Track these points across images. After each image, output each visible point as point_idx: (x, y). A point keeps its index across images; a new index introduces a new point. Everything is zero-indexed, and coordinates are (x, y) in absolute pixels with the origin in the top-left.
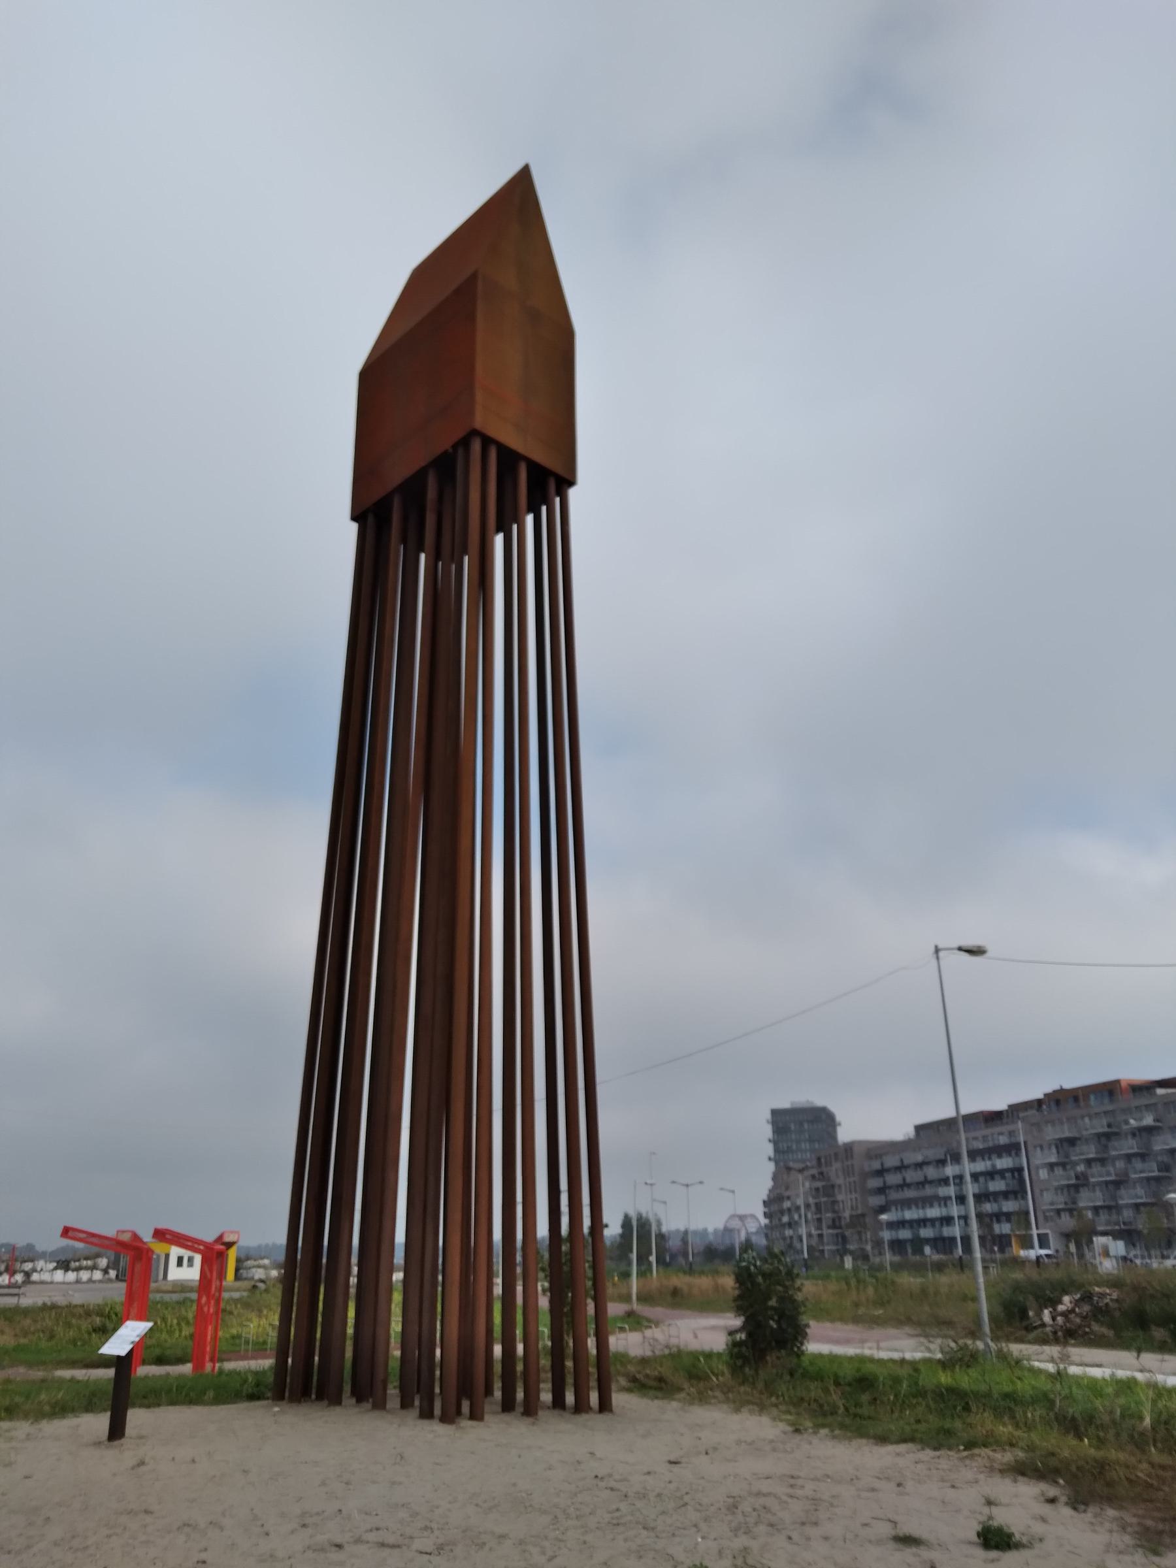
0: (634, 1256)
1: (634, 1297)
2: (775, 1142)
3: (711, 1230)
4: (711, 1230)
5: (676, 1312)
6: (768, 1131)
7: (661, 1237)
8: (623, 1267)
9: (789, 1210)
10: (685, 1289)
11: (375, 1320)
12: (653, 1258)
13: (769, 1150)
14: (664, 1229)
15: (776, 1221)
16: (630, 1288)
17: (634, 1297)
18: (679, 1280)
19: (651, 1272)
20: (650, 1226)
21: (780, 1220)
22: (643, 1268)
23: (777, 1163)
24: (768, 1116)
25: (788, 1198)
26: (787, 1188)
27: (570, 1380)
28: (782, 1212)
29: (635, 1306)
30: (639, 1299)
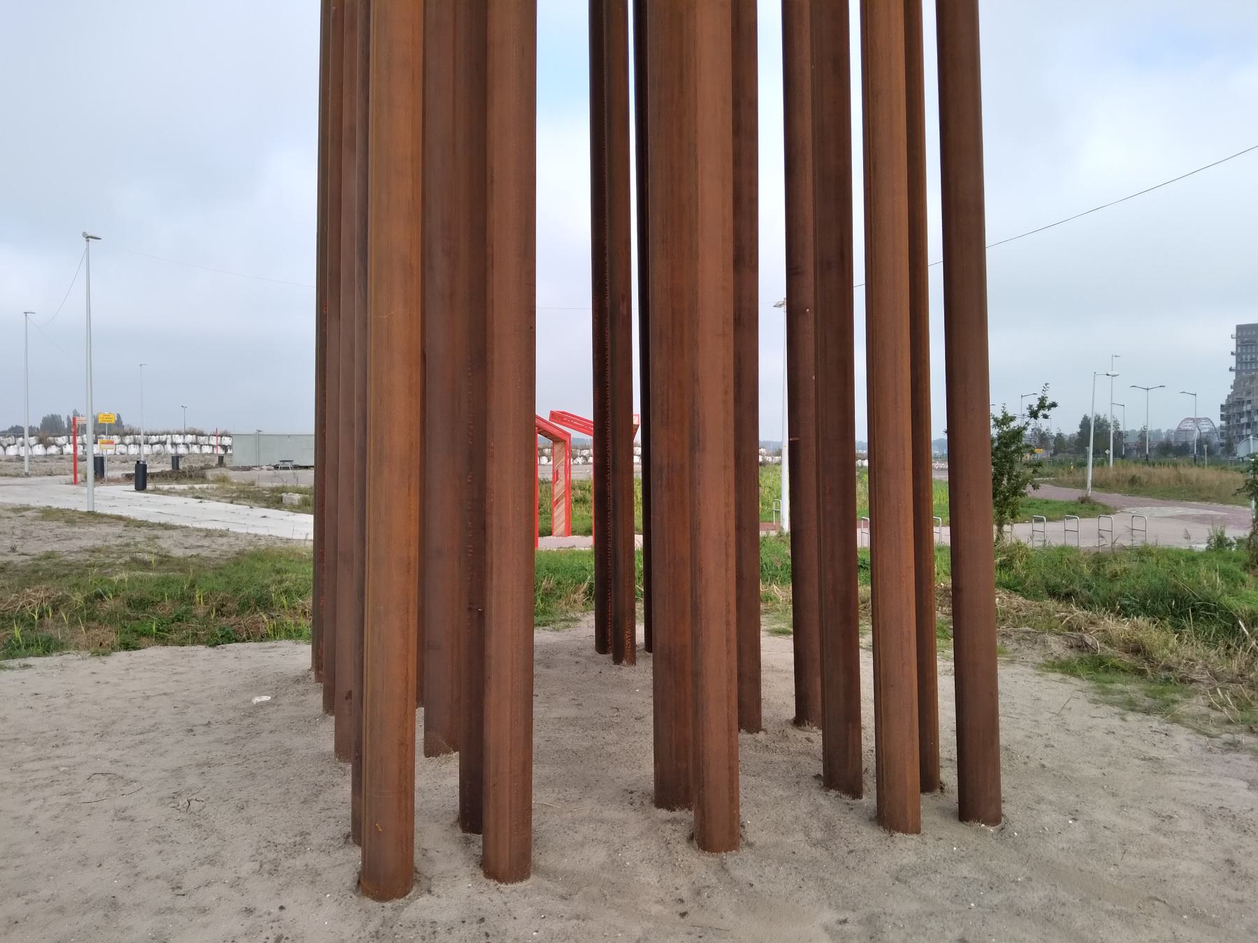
0: (1091, 449)
1: (1089, 484)
2: (1238, 355)
3: (1164, 431)
4: (1164, 431)
5: (1135, 499)
6: (1232, 345)
7: (1119, 435)
8: (1080, 459)
9: (1249, 412)
10: (1145, 478)
11: (424, 493)
12: (1110, 452)
13: (1232, 361)
14: (1121, 429)
15: (1233, 422)
16: (1085, 475)
17: (1089, 484)
18: (1134, 470)
19: (1108, 461)
20: (1109, 426)
21: (1238, 421)
22: (1099, 459)
23: (1238, 372)
24: (1234, 332)
25: (1249, 402)
26: (1249, 393)
27: (942, 615)
28: (1241, 415)
29: (1090, 492)
30: (1094, 486)
